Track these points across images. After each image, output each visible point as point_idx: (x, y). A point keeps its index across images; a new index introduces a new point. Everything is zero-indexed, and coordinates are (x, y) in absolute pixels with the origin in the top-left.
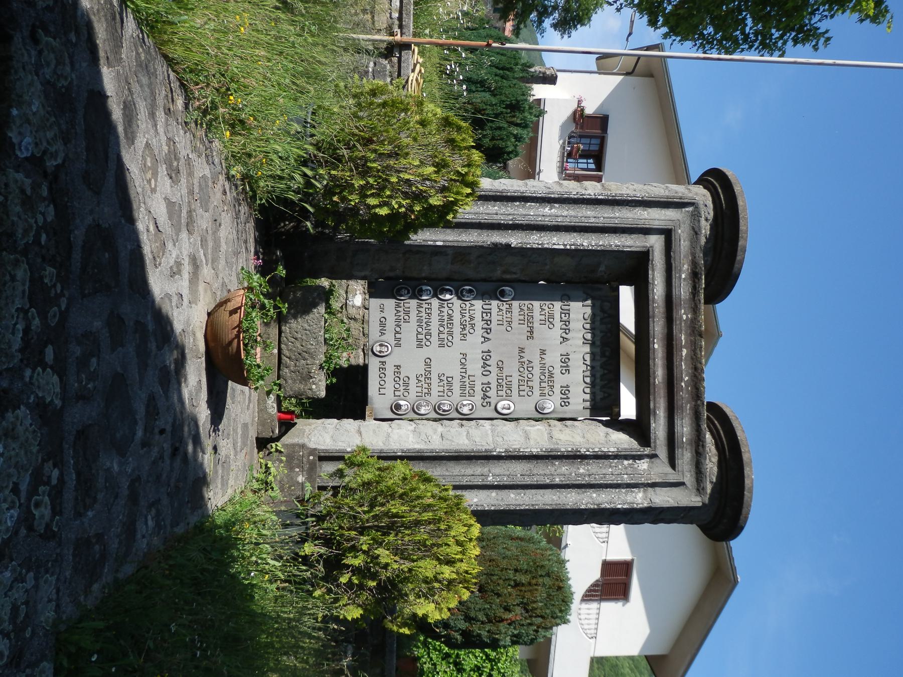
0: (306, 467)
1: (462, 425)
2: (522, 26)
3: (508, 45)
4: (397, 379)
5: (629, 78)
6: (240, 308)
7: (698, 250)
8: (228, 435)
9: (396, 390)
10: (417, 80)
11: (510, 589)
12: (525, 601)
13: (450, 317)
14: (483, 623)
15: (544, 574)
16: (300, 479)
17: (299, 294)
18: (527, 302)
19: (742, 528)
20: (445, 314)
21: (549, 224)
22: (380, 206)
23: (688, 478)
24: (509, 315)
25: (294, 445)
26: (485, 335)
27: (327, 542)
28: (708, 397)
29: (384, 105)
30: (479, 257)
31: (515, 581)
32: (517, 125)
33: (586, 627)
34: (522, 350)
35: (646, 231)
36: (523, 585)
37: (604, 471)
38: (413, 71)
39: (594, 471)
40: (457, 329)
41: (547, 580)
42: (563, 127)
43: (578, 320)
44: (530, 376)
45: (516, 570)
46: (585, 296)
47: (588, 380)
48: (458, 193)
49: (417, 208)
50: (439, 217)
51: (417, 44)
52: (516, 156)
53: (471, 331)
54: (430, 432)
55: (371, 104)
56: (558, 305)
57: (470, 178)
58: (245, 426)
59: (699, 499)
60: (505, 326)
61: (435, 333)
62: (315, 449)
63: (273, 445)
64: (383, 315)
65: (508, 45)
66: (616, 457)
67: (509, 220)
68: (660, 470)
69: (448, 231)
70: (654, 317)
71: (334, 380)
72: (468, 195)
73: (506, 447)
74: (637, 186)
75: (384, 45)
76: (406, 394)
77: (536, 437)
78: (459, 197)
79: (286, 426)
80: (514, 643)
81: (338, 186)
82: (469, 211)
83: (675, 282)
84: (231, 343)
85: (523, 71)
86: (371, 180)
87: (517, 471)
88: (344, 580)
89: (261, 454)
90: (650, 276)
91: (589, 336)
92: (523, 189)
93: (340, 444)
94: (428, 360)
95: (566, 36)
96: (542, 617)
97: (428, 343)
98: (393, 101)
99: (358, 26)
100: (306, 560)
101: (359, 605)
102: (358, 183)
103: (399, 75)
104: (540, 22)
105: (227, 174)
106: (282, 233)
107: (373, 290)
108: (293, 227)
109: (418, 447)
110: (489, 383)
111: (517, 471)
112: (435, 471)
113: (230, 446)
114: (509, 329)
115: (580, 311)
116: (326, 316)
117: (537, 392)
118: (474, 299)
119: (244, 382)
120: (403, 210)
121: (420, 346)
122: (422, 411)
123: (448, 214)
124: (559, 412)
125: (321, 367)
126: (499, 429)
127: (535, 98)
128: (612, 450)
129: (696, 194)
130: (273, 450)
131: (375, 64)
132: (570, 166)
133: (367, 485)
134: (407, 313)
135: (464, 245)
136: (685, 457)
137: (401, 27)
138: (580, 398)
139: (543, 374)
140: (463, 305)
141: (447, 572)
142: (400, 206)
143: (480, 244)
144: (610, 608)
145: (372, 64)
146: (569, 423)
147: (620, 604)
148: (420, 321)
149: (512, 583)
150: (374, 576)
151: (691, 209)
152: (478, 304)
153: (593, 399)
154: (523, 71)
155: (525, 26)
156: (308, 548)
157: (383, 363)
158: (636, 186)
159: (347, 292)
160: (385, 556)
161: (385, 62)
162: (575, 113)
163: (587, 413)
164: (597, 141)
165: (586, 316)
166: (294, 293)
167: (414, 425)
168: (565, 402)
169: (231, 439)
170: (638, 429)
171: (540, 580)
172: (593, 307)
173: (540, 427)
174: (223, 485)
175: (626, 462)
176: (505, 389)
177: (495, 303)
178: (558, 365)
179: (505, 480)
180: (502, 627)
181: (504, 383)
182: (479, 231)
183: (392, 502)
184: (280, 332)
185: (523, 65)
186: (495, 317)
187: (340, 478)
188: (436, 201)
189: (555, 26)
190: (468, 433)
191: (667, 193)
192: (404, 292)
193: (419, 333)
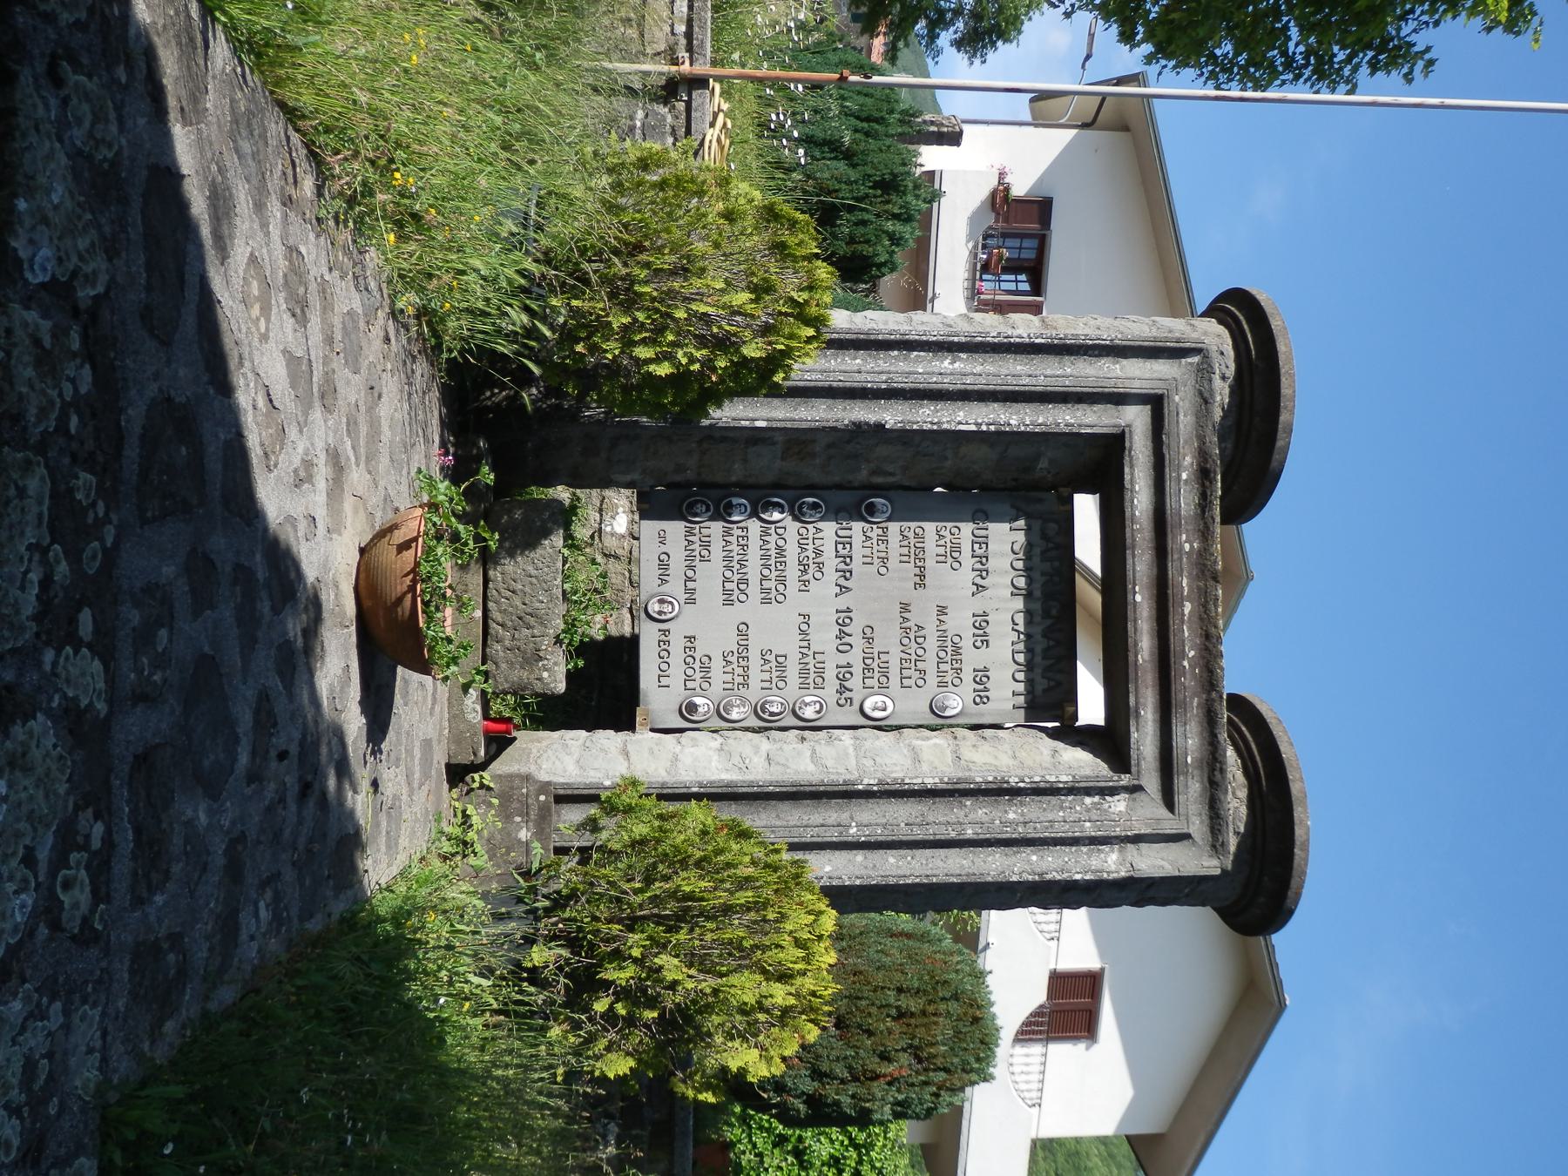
1: (803, 739)
2: (901, 44)
3: (876, 79)
4: (689, 660)
5: (1088, 132)
6: (415, 539)
7: (1209, 430)
8: (398, 759)
9: (688, 678)
10: (719, 140)
11: (889, 1023)
12: (916, 1042)
13: (781, 551)
14: (843, 1081)
15: (948, 995)
16: (524, 835)
17: (518, 515)
18: (913, 525)
19: (1291, 913)
20: (772, 546)
21: (951, 388)
22: (657, 360)
23: (1197, 826)
24: (882, 547)
25: (511, 777)
26: (842, 582)
27: (573, 943)
29: (662, 185)
30: (829, 446)
31: (898, 1008)
32: (896, 217)
34: (905, 607)
36: (912, 1015)
38: (712, 125)
39: (1033, 816)
40: (792, 572)
41: (953, 1006)
42: (974, 219)
43: (1003, 555)
44: (920, 652)
45: (900, 990)
46: (1014, 512)
47: (1021, 658)
48: (791, 337)
49: (721, 363)
50: (759, 378)
51: (718, 79)
52: (892, 270)
53: (818, 575)
54: (748, 751)
56: (967, 528)
57: (813, 310)
59: (1215, 862)
60: (874, 569)
62: (549, 783)
63: (476, 776)
64: (664, 548)
65: (876, 79)
67: (880, 381)
68: (1146, 812)
69: (776, 402)
70: (1133, 548)
71: (581, 663)
72: (809, 340)
76: (705, 686)
77: (933, 759)
78: (794, 344)
79: (498, 743)
80: (898, 1116)
81: (584, 326)
82: (810, 367)
86: (641, 316)
87: (899, 818)
88: (600, 1006)
90: (1127, 477)
91: (1021, 582)
92: (905, 328)
93: (592, 773)
94: (743, 627)
95: (977, 61)
97: (743, 598)
98: (678, 179)
101: (628, 1054)
102: (619, 320)
103: (688, 132)
104: (933, 37)
107: (646, 506)
108: (507, 398)
110: (849, 665)
111: (899, 818)
112: (757, 819)
113: (402, 779)
114: (883, 570)
115: (1006, 539)
116: (566, 552)
117: (932, 679)
118: (822, 519)
120: (696, 367)
121: (728, 602)
122: (734, 715)
123: (774, 372)
124: (972, 715)
125: (558, 641)
126: (868, 744)
128: (1064, 778)
129: (1205, 333)
130: (476, 785)
132: (986, 286)
133: (638, 844)
134: (706, 545)
136: (1191, 790)
138: (1007, 690)
139: (943, 648)
140: (803, 531)
141: (780, 995)
142: (692, 360)
143: (831, 424)
144: (1064, 1053)
145: (640, 114)
146: (988, 732)
147: (1082, 1046)
148: (729, 559)
149: (894, 1012)
151: (1196, 359)
152: (829, 528)
153: (1030, 691)
155: (907, 45)
156: (539, 955)
157: (665, 632)
160: (671, 967)
162: (994, 194)
164: (1034, 243)
165: (1017, 548)
166: (509, 512)
167: (720, 740)
168: (982, 697)
169: (402, 767)
170: (1109, 742)
171: (942, 1007)
172: (1028, 531)
173: (939, 739)
174: (389, 847)
175: (1088, 800)
176: (877, 675)
177: (857, 527)
178: (968, 634)
179: (879, 834)
180: (878, 1088)
181: (875, 666)
182: (830, 401)
183: (684, 874)
185: (903, 112)
186: (858, 551)
188: (753, 350)
189: (958, 44)
190: (814, 751)
191: (1154, 333)
192: (700, 508)
193: (726, 580)
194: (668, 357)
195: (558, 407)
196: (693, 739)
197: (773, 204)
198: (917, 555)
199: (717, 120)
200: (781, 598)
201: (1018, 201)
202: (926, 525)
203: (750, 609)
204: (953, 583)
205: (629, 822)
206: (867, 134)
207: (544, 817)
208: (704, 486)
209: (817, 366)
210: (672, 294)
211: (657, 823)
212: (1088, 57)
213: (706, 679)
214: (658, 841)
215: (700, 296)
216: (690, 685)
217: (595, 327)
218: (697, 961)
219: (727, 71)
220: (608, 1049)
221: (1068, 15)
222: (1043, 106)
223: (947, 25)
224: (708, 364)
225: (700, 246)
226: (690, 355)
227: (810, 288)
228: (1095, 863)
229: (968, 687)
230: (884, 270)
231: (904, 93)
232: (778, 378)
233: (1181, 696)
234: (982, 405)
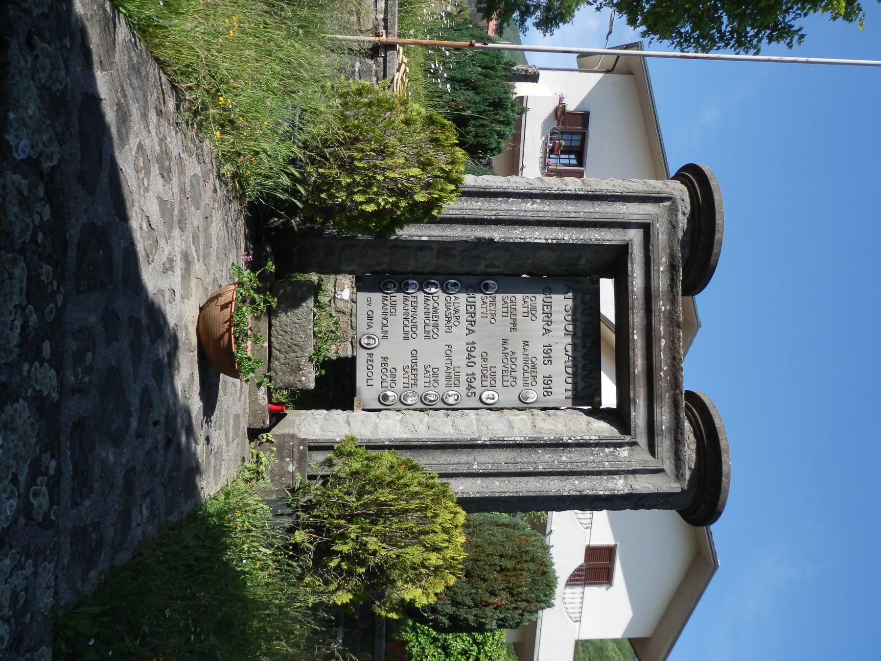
0: (297, 456)
1: (448, 415)
2: (505, 25)
4: (384, 370)
5: (608, 75)
6: (231, 303)
8: (221, 426)
9: (383, 381)
10: (402, 79)
11: (495, 574)
12: (510, 585)
13: (436, 310)
14: (469, 607)
15: (528, 559)
16: (291, 468)
18: (510, 295)
19: (720, 513)
20: (431, 307)
22: (369, 201)
24: (493, 308)
25: (284, 436)
26: (470, 327)
27: (318, 529)
29: (370, 105)
30: (463, 251)
32: (501, 122)
33: (571, 611)
34: (505, 342)
35: (625, 225)
36: (508, 570)
37: (586, 459)
38: (398, 70)
40: (442, 322)
41: (531, 565)
42: (545, 124)
43: (560, 312)
44: (513, 367)
45: (502, 556)
47: (570, 370)
49: (403, 204)
50: (424, 213)
51: (402, 45)
52: (499, 152)
53: (457, 323)
54: (417, 422)
56: (540, 297)
59: (678, 485)
60: (487, 320)
62: (305, 439)
63: (265, 435)
64: (370, 308)
65: (490, 45)
66: (598, 444)
68: (640, 457)
69: (433, 226)
70: (633, 309)
71: (323, 372)
72: (452, 192)
73: (490, 436)
77: (520, 426)
79: (277, 417)
80: (500, 627)
82: (453, 207)
83: (653, 274)
84: (222, 336)
85: (505, 69)
86: (358, 178)
87: (502, 459)
90: (630, 269)
91: (570, 328)
92: (505, 185)
93: (330, 434)
94: (414, 352)
96: (527, 601)
97: (414, 336)
98: (378, 100)
99: (345, 28)
101: (349, 591)
102: (345, 180)
104: (523, 21)
106: (272, 229)
107: (360, 284)
108: (282, 223)
109: (405, 436)
110: (474, 374)
111: (502, 459)
113: (223, 436)
114: (493, 321)
115: (562, 303)
116: (315, 310)
117: (520, 382)
118: (459, 292)
121: (406, 338)
122: (409, 402)
123: (432, 209)
125: (311, 360)
126: (484, 418)
128: (593, 438)
129: (674, 189)
130: (264, 440)
132: (552, 161)
133: (354, 474)
134: (394, 306)
135: (449, 239)
136: (664, 444)
137: (386, 28)
138: (562, 388)
139: (526, 365)
140: (448, 299)
141: (434, 559)
142: (387, 203)
143: (464, 239)
144: (594, 592)
145: (358, 64)
146: (551, 412)
147: (604, 588)
148: (406, 314)
149: (498, 568)
150: (362, 563)
151: (668, 203)
152: (463, 297)
154: (505, 69)
155: (508, 25)
156: (300, 536)
157: (371, 355)
158: (615, 182)
160: (373, 543)
161: (370, 62)
162: (556, 110)
165: (568, 308)
167: (401, 415)
168: (548, 392)
169: (223, 430)
170: (619, 417)
171: (525, 566)
173: (523, 416)
174: (215, 474)
175: (607, 450)
176: (489, 379)
177: (479, 296)
179: (490, 468)
180: (489, 611)
181: (488, 374)
182: (463, 226)
183: (381, 491)
184: (270, 326)
185: (505, 63)
186: (479, 310)
188: (421, 197)
189: (537, 25)
190: (454, 422)
191: (645, 188)
192: (390, 285)
193: (405, 326)
195: (312, 229)
196: (386, 415)
197: (432, 115)
201: (571, 114)
203: (418, 342)
206: (485, 76)
207: (301, 461)
209: (456, 206)
212: (610, 33)
213: (394, 381)
218: (388, 539)
224: (395, 205)
226: (385, 201)
227: (453, 163)
228: (610, 485)
229: (540, 386)
230: (495, 152)
231: (506, 53)
232: (435, 212)
233: (659, 392)
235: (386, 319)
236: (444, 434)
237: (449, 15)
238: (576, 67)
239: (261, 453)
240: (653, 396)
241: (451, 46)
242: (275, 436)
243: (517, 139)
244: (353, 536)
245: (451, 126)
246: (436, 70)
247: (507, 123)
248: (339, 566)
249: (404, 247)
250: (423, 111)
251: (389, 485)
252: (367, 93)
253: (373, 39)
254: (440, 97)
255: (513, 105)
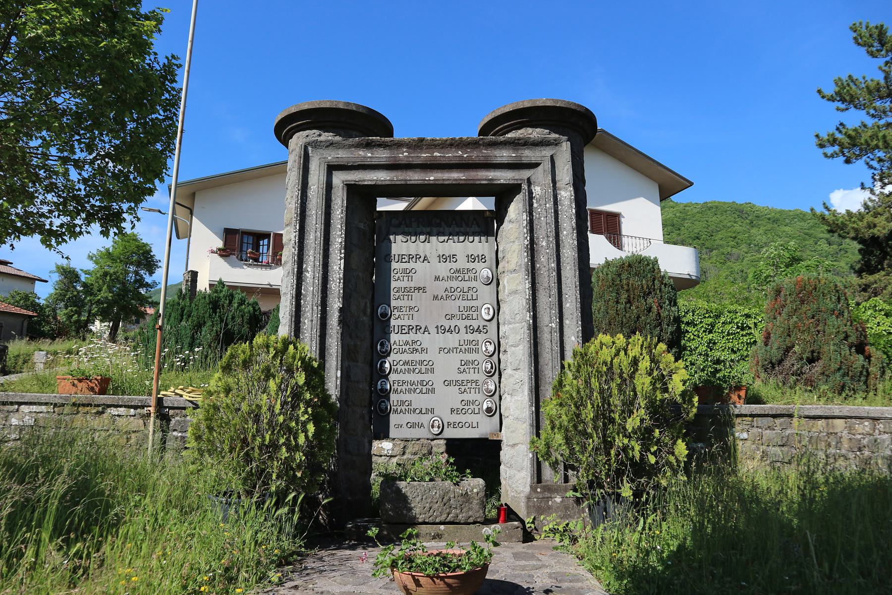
0: (547, 494)
1: (505, 351)
2: (150, 300)
3: (161, 311)
4: (463, 411)
5: (195, 212)
6: (413, 577)
7: (347, 142)
8: (529, 576)
9: (473, 412)
10: (189, 393)
11: (633, 308)
12: (642, 294)
13: (406, 363)
14: (661, 330)
15: (619, 279)
16: (558, 500)
17: (389, 506)
18: (392, 293)
19: (587, 109)
20: (403, 367)
21: (321, 272)
22: (305, 431)
23: (547, 152)
24: (404, 309)
25: (528, 507)
26: (422, 331)
27: (619, 473)
28: (475, 135)
29: (210, 429)
30: (351, 337)
31: (626, 303)
32: (230, 302)
33: (642, 247)
34: (436, 298)
35: (329, 187)
36: (629, 296)
37: (544, 224)
38: (181, 396)
39: (544, 233)
40: (417, 357)
41: (624, 276)
42: (233, 265)
43: (408, 247)
44: (459, 290)
45: (617, 302)
46: (386, 241)
47: (462, 238)
48: (294, 358)
49: (308, 396)
50: (316, 374)
51: (158, 392)
52: (257, 304)
53: (419, 343)
54: (512, 380)
55: (209, 440)
56: (394, 265)
57: (279, 345)
58: (516, 556)
59: (564, 144)
60: (415, 314)
61: (420, 377)
62: (531, 487)
63: (528, 526)
64: (404, 425)
65: (161, 311)
66: (530, 213)
67: (317, 310)
68: (540, 176)
69: (327, 365)
70: (406, 180)
71: (468, 471)
72: (296, 348)
73: (524, 312)
74: (289, 194)
75: (158, 421)
76: (477, 403)
77: (515, 284)
78: (298, 356)
79: (509, 514)
80: (675, 304)
81: (287, 472)
82: (309, 346)
83: (375, 162)
84: (448, 585)
85: (184, 299)
86: (282, 441)
87: (546, 301)
88: (652, 460)
89: (537, 537)
90: (370, 183)
91: (422, 238)
92: (289, 296)
93: (525, 463)
94: (446, 383)
95: (160, 264)
96: (654, 281)
97: (430, 383)
98: (206, 420)
99: (141, 444)
100: (637, 494)
101: (674, 443)
102: (284, 453)
103: (184, 408)
104: (147, 285)
105: (278, 585)
106: (330, 521)
107: (382, 435)
108: (324, 511)
109: (526, 392)
110: (466, 327)
111: (546, 301)
112: (550, 374)
113: (538, 573)
114: (416, 309)
115: (400, 245)
116: (409, 480)
117: (473, 284)
118: (389, 341)
119: (485, 567)
120: (309, 410)
121: (433, 391)
122: (492, 388)
123: (312, 367)
124: (491, 264)
125: (457, 484)
126: (508, 318)
127: (208, 289)
128: (525, 217)
129: (297, 144)
130: (533, 526)
131: (175, 430)
132: (265, 260)
133: (568, 440)
134: (403, 403)
135: (340, 350)
136: (529, 155)
137: (143, 407)
138: (478, 246)
139: (457, 278)
140: (395, 351)
141: (645, 364)
142: (306, 412)
143: (339, 336)
144: (626, 228)
145: (175, 433)
146: (500, 255)
147: (622, 220)
148: (410, 391)
149: (628, 305)
150: (649, 431)
151: (310, 149)
152: (394, 337)
153: (479, 234)
154: (184, 299)
155: (151, 297)
156: (626, 491)
157: (449, 424)
158: (288, 196)
159: (381, 456)
160: (632, 423)
161: (173, 421)
162: (221, 256)
163: (492, 239)
164: (245, 237)
165: (405, 240)
166: (387, 511)
167: (506, 395)
168: (482, 259)
169: (532, 572)
170: (504, 195)
171: (625, 282)
172: (396, 234)
173: (505, 281)
174: (578, 581)
175: (535, 205)
176: (471, 313)
177: (393, 322)
178: (449, 265)
179: (555, 311)
180: (664, 314)
181: (466, 314)
182: (327, 337)
183: (584, 416)
184: (424, 523)
185: (179, 299)
186: (406, 322)
187: (558, 464)
188: (301, 378)
189: (151, 273)
190: (512, 346)
191: (296, 169)
192: (383, 406)
193: (421, 392)
194: (304, 424)
195: (329, 482)
196: (506, 409)
197: (222, 367)
198: (408, 292)
199: (177, 393)
200: (431, 363)
201: (225, 244)
202: (392, 286)
203: (437, 379)
204: (423, 272)
205: (555, 444)
206: (189, 316)
207: (551, 489)
208: (371, 403)
209: (309, 343)
210: (270, 423)
211: (556, 430)
212: (160, 212)
213: (473, 402)
214: (567, 430)
215: (271, 408)
216: (477, 411)
217: (287, 467)
218: (629, 408)
219: (154, 388)
220: (673, 454)
221: (139, 220)
222: (180, 231)
223: (142, 278)
224: (308, 403)
225: (244, 407)
226: (303, 413)
227: (268, 347)
228: (567, 203)
229: (477, 265)
230: (257, 308)
231: (169, 299)
232: (315, 364)
233: (482, 158)
234: (330, 257)
235: (415, 411)
236: (523, 355)
237: (135, 349)
238: (187, 239)
239: (544, 528)
240: (485, 164)
241: (160, 347)
242: (528, 516)
243: (249, 290)
244: (626, 441)
245: (233, 348)
246: (183, 360)
247: (231, 297)
248: (654, 454)
249: (347, 394)
250: (217, 375)
251: (577, 408)
252: (199, 430)
253: (152, 419)
254: (206, 357)
255: (216, 292)
